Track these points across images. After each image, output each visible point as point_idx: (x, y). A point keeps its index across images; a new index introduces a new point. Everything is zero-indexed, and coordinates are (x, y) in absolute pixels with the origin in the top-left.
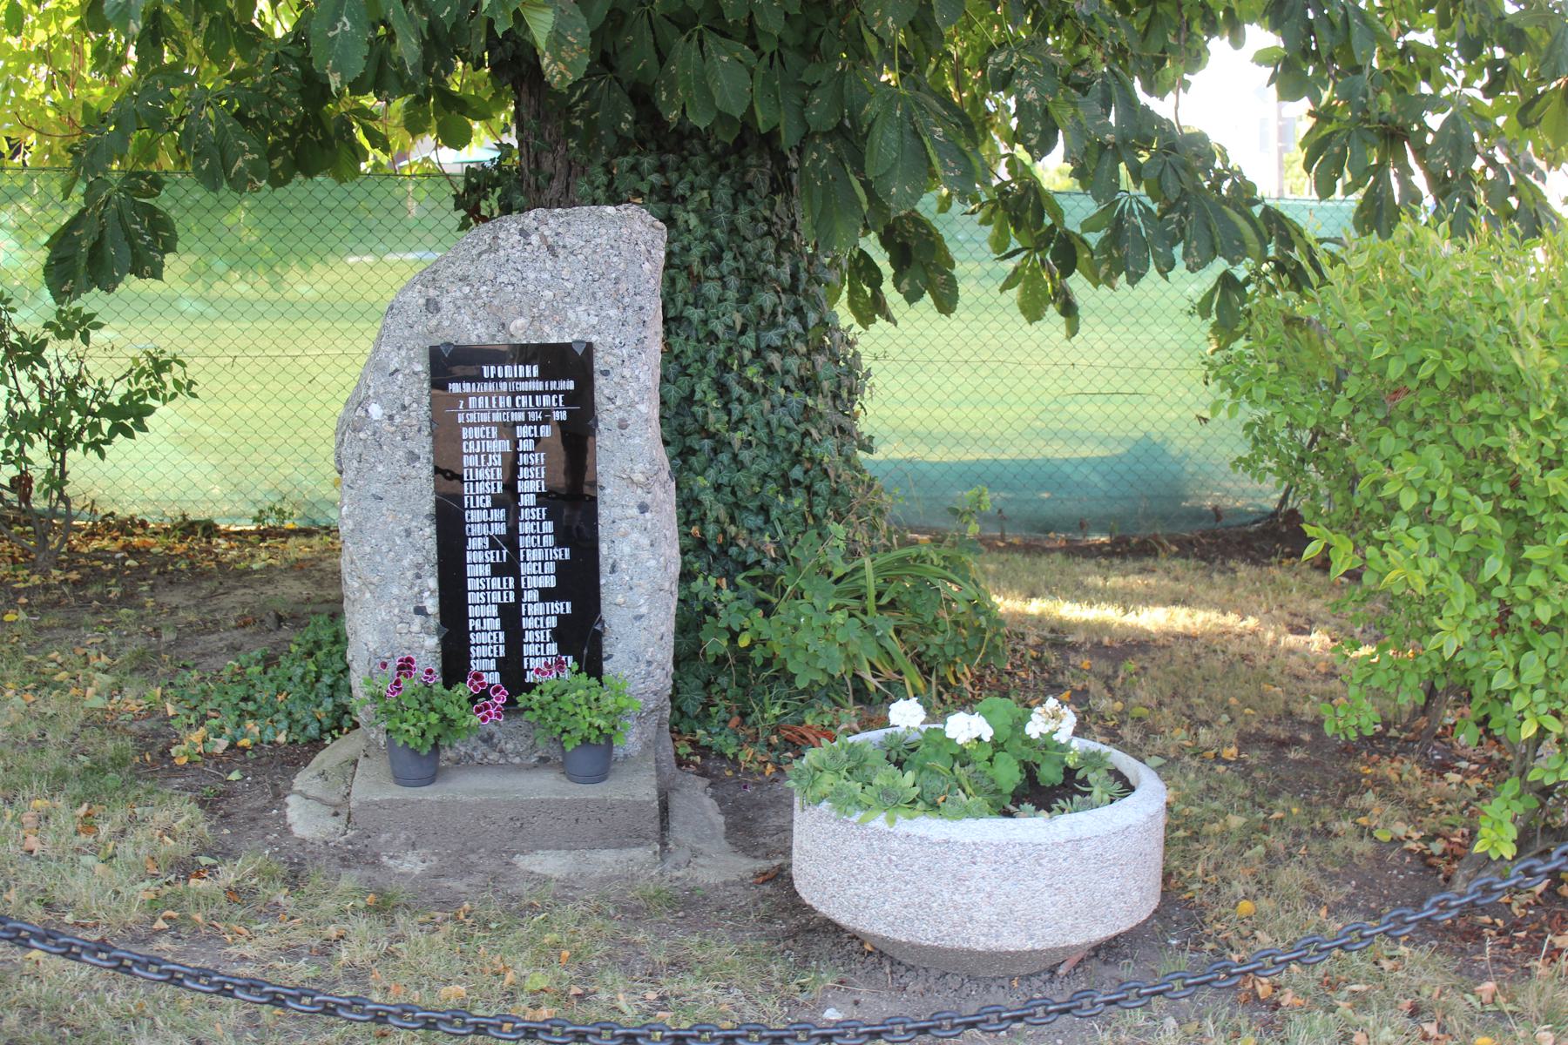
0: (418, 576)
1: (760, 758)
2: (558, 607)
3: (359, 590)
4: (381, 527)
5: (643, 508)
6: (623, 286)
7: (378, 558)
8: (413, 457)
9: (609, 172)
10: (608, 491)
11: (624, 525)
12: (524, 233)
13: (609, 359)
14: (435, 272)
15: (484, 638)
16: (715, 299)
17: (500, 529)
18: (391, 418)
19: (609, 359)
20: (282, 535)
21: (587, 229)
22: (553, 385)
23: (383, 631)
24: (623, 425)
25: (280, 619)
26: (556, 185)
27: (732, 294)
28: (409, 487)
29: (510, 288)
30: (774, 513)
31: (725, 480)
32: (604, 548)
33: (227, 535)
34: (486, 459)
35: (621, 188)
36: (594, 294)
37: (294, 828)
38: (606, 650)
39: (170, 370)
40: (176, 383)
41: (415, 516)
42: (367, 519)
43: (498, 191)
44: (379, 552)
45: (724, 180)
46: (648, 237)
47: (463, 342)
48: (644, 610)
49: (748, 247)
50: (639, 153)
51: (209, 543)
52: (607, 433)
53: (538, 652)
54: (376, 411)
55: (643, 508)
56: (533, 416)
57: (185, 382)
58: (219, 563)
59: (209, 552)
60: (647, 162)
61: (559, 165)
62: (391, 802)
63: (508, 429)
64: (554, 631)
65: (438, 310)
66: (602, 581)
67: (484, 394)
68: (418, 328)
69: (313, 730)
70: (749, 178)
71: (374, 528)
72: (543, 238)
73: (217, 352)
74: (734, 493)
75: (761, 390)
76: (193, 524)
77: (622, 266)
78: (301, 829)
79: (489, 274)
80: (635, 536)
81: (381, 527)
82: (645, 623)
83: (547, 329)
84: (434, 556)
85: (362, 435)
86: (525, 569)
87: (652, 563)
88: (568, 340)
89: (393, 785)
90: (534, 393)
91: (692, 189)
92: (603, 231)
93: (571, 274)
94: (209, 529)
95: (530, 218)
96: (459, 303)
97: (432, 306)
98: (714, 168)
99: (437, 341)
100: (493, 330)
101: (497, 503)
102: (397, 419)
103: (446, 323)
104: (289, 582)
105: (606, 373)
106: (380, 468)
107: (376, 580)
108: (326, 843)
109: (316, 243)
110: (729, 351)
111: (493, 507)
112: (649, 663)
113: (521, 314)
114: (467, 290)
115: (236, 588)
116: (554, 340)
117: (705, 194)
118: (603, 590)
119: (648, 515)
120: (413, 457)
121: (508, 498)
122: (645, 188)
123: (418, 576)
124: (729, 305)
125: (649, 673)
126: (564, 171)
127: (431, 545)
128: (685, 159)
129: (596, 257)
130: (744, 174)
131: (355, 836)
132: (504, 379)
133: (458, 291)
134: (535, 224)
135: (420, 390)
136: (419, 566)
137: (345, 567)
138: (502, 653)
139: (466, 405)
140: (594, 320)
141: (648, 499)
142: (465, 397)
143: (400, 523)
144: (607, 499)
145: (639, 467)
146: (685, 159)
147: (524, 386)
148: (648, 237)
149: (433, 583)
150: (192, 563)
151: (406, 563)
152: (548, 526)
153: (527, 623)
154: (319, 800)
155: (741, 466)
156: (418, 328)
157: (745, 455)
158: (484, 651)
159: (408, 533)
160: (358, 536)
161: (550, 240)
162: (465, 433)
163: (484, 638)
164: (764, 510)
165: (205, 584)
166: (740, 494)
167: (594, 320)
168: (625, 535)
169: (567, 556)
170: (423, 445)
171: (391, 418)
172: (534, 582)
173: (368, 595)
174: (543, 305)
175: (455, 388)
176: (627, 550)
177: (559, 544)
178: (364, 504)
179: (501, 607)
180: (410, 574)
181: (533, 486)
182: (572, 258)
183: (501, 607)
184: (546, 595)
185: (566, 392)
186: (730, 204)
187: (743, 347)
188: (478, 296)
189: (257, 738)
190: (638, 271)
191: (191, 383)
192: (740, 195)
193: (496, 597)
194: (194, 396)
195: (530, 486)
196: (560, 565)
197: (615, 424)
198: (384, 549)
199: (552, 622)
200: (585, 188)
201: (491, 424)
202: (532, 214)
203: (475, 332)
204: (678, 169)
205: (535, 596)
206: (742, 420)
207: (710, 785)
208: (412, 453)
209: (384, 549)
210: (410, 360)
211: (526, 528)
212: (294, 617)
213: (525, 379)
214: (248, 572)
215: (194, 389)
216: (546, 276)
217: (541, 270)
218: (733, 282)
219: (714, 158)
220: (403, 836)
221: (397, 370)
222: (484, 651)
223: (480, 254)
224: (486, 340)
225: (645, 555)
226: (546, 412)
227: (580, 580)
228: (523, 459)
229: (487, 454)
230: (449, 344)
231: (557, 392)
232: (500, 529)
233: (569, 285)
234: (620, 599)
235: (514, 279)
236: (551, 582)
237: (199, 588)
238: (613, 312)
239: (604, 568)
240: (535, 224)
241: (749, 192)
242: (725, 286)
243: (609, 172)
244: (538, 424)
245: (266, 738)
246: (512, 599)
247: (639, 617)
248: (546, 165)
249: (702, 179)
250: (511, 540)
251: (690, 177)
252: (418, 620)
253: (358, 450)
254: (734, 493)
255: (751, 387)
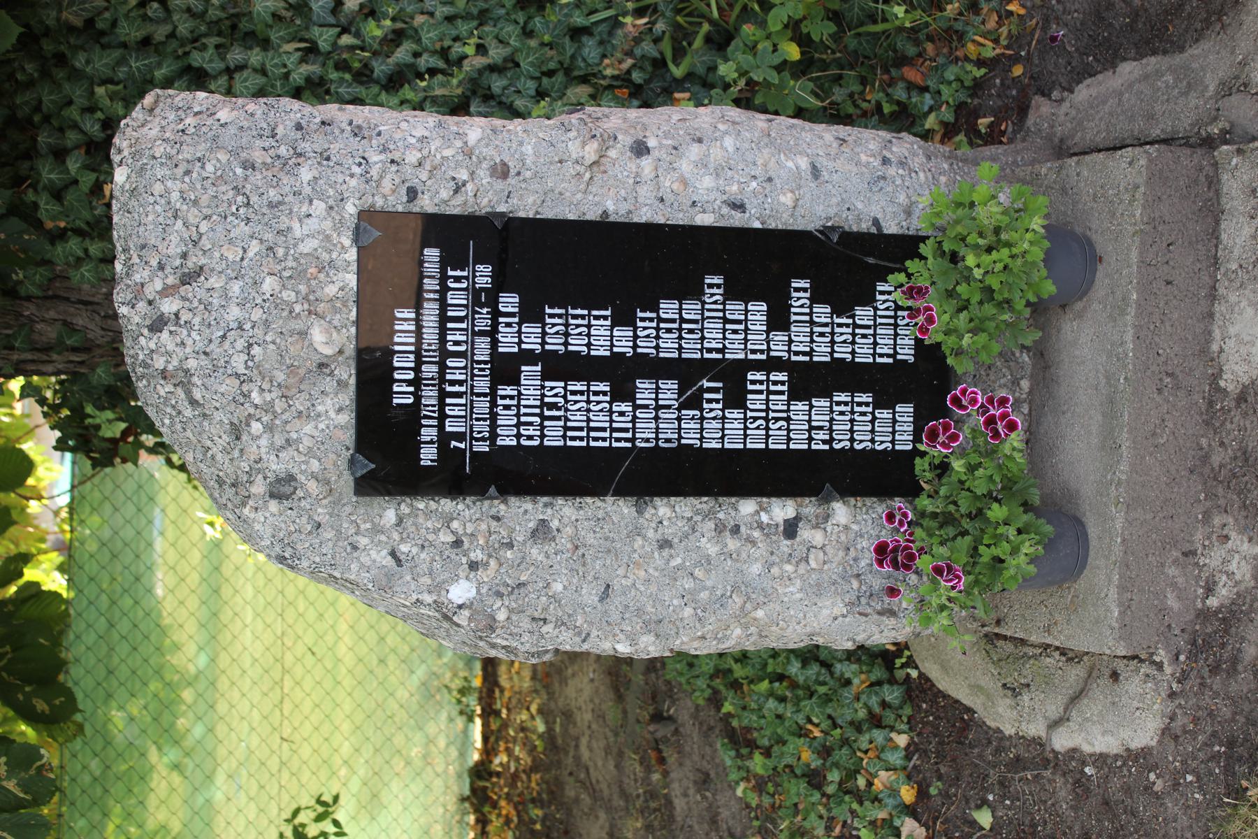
0: (736, 530)
1: (992, 24)
2: (799, 300)
3: (745, 627)
4: (653, 589)
5: (640, 149)
6: (258, 156)
7: (704, 595)
8: (542, 532)
9: (61, 235)
10: (610, 206)
11: (667, 182)
12: (158, 325)
13: (387, 185)
14: (220, 482)
15: (841, 427)
16: (263, 80)
17: (669, 388)
18: (473, 566)
19: (387, 185)
20: (491, 693)
21: (153, 215)
22: (431, 284)
23: (819, 590)
24: (502, 171)
25: (658, 717)
26: (81, 320)
27: (255, 57)
28: (590, 539)
29: (256, 350)
30: (579, 20)
31: (531, 86)
32: (705, 219)
33: (489, 751)
34: (553, 406)
35: (86, 215)
36: (271, 205)
37: (1136, 744)
38: (865, 226)
39: (303, 825)
40: (319, 818)
41: (639, 532)
42: (640, 611)
43: (89, 409)
44: (692, 592)
45: (79, 61)
46: (172, 116)
47: (349, 437)
48: (804, 163)
49: (184, 28)
50: (34, 186)
51: (498, 774)
52: (514, 201)
53: (879, 333)
54: (461, 592)
55: (640, 149)
56: (483, 323)
57: (320, 809)
58: (534, 768)
59: (515, 777)
60: (49, 173)
61: (52, 314)
62: (1122, 589)
63: (505, 370)
64: (838, 311)
65: (291, 478)
66: (757, 225)
67: (442, 405)
68: (321, 514)
69: (892, 694)
70: (78, 22)
71: (655, 600)
72: (166, 291)
73: (275, 759)
74: (550, 74)
75: (399, 25)
76: (473, 790)
77: (223, 157)
78: (1143, 732)
79: (229, 386)
80: (685, 166)
81: (653, 589)
82: (823, 162)
83: (331, 290)
84: (704, 504)
85: (501, 616)
86: (736, 353)
87: (729, 142)
88: (352, 255)
89: (1081, 584)
90: (443, 319)
91: (91, 110)
92: (158, 188)
93: (230, 244)
94: (480, 772)
95: (131, 315)
96: (279, 440)
97: (283, 488)
98: (60, 74)
99: (346, 483)
100: (329, 384)
101: (622, 392)
102: (477, 555)
103: (315, 465)
104: (570, 691)
105: (412, 194)
106: (558, 587)
107: (738, 600)
108: (1172, 695)
109: (141, 634)
110: (342, 66)
111: (633, 400)
112: (885, 161)
113: (303, 334)
114: (256, 427)
115: (577, 758)
116: (352, 280)
117: (100, 91)
118: (772, 225)
119: (652, 143)
120: (542, 532)
121: (621, 374)
122: (87, 180)
123: (736, 530)
124: (271, 61)
125: (902, 164)
126: (62, 307)
127: (686, 506)
128: (47, 119)
129: (205, 200)
130: (71, 29)
131: (1166, 648)
132: (417, 369)
133: (259, 441)
134: (141, 306)
135: (428, 514)
136: (720, 528)
137: (709, 648)
138: (866, 398)
139: (460, 437)
140: (319, 207)
141: (625, 140)
142: (444, 438)
143: (647, 557)
144: (623, 208)
145: (574, 149)
146: (47, 119)
147: (430, 335)
148: (172, 116)
149: (747, 507)
150: (533, 801)
151: (713, 550)
152: (668, 308)
153: (822, 355)
154: (1075, 699)
155: (511, 63)
156: (321, 514)
157: (496, 54)
158: (862, 429)
159: (665, 544)
160: (666, 628)
161: (171, 280)
162: (506, 440)
163: (841, 427)
164: (577, 33)
165: (570, 793)
166: (552, 65)
167: (319, 207)
168: (684, 182)
169: (717, 280)
170: (522, 512)
171: (473, 566)
172: (757, 339)
173: (760, 614)
174: (289, 295)
175: (428, 455)
176: (708, 181)
177: (696, 293)
178: (615, 617)
179: (795, 394)
180: (732, 544)
181: (601, 329)
182: (206, 243)
183: (795, 394)
184: (779, 320)
185: (444, 264)
186: (117, 54)
187: (335, 44)
188: (268, 408)
189: (902, 775)
190: (232, 130)
191: (319, 802)
192: (105, 40)
193: (779, 403)
194: (336, 799)
195: (599, 335)
196: (731, 293)
197: (499, 185)
198: (689, 584)
199: (822, 312)
200: (86, 271)
201: (493, 394)
202: (123, 310)
203: (335, 413)
204: (61, 130)
205: (779, 337)
206: (444, 53)
207: (1046, 94)
208: (534, 533)
209: (689, 584)
210: (377, 530)
211: (668, 347)
212: (654, 698)
213: (419, 332)
214: (549, 737)
215: (327, 798)
216: (236, 288)
217: (225, 296)
218: (236, 55)
219: (45, 74)
220: (1172, 571)
221: (393, 554)
222: (862, 429)
223: (193, 403)
224: (347, 397)
225: (716, 154)
226: (475, 295)
227: (759, 261)
228: (555, 344)
229: (543, 405)
230: (352, 462)
231: (444, 278)
232: (669, 388)
233: (254, 247)
234: (787, 199)
235: (240, 344)
236: (759, 309)
237: (577, 800)
238: (306, 174)
239: (737, 220)
240: (141, 306)
241: (100, 25)
242: (241, 68)
243: (61, 235)
244: (496, 314)
245: (899, 762)
246: (782, 377)
247: (815, 172)
248: (50, 333)
249: (78, 94)
250: (687, 372)
251: (73, 113)
252: (805, 533)
253: (526, 624)
254: (550, 74)
255: (396, 38)
